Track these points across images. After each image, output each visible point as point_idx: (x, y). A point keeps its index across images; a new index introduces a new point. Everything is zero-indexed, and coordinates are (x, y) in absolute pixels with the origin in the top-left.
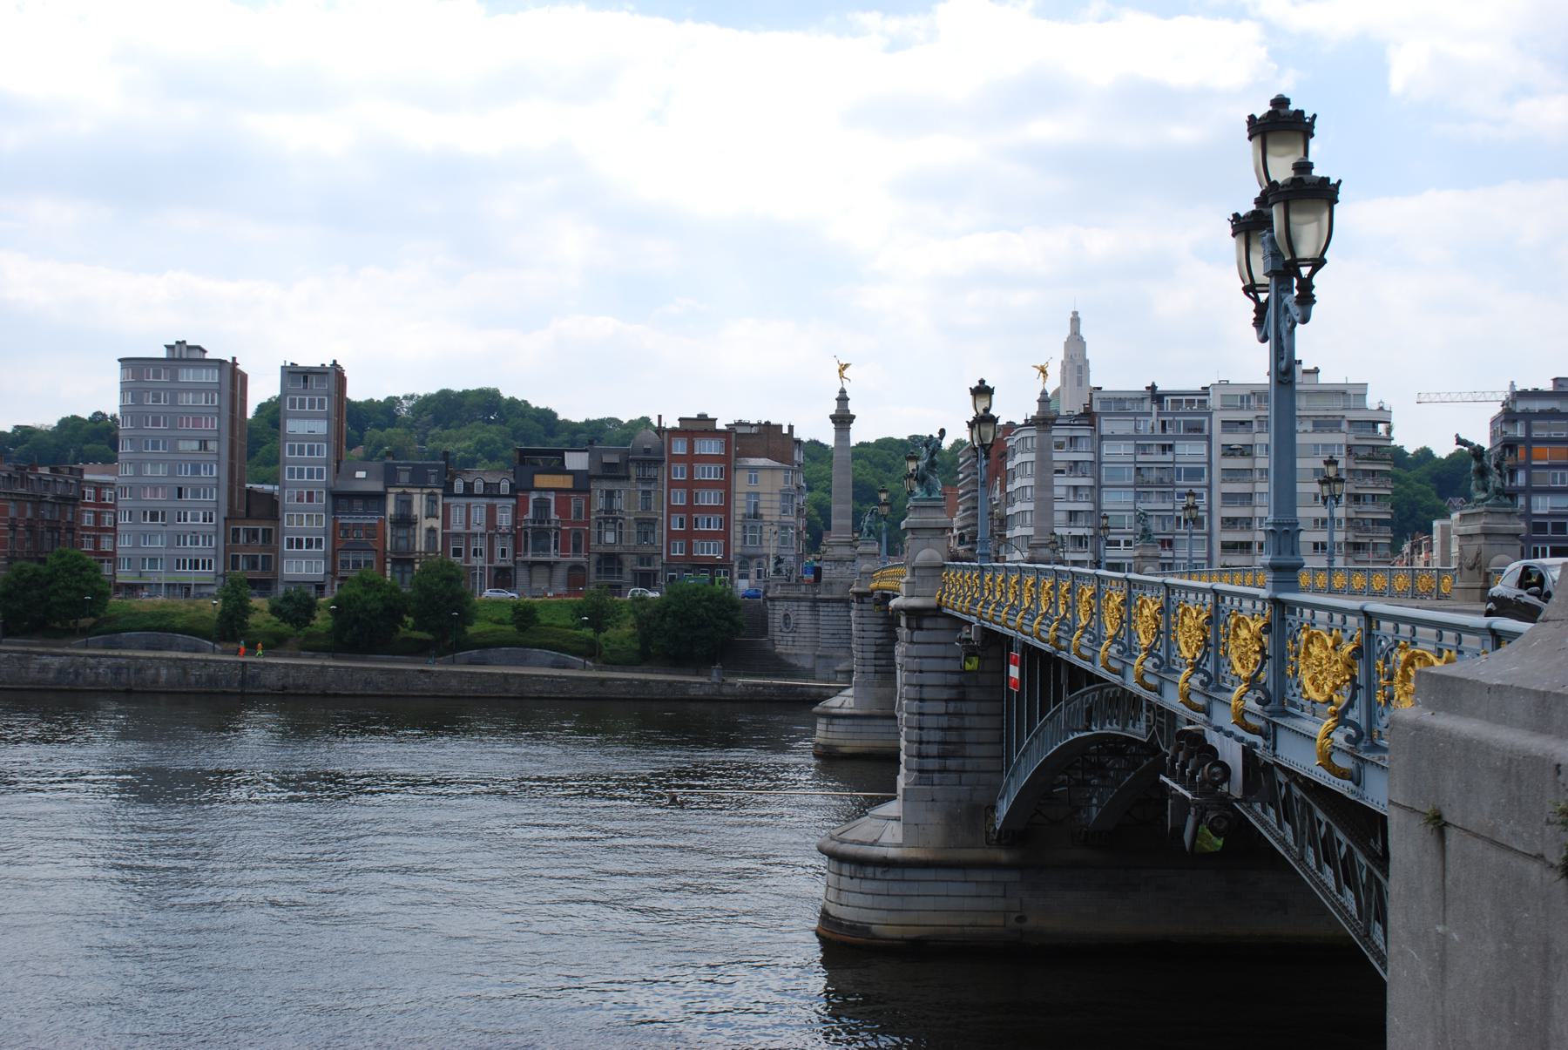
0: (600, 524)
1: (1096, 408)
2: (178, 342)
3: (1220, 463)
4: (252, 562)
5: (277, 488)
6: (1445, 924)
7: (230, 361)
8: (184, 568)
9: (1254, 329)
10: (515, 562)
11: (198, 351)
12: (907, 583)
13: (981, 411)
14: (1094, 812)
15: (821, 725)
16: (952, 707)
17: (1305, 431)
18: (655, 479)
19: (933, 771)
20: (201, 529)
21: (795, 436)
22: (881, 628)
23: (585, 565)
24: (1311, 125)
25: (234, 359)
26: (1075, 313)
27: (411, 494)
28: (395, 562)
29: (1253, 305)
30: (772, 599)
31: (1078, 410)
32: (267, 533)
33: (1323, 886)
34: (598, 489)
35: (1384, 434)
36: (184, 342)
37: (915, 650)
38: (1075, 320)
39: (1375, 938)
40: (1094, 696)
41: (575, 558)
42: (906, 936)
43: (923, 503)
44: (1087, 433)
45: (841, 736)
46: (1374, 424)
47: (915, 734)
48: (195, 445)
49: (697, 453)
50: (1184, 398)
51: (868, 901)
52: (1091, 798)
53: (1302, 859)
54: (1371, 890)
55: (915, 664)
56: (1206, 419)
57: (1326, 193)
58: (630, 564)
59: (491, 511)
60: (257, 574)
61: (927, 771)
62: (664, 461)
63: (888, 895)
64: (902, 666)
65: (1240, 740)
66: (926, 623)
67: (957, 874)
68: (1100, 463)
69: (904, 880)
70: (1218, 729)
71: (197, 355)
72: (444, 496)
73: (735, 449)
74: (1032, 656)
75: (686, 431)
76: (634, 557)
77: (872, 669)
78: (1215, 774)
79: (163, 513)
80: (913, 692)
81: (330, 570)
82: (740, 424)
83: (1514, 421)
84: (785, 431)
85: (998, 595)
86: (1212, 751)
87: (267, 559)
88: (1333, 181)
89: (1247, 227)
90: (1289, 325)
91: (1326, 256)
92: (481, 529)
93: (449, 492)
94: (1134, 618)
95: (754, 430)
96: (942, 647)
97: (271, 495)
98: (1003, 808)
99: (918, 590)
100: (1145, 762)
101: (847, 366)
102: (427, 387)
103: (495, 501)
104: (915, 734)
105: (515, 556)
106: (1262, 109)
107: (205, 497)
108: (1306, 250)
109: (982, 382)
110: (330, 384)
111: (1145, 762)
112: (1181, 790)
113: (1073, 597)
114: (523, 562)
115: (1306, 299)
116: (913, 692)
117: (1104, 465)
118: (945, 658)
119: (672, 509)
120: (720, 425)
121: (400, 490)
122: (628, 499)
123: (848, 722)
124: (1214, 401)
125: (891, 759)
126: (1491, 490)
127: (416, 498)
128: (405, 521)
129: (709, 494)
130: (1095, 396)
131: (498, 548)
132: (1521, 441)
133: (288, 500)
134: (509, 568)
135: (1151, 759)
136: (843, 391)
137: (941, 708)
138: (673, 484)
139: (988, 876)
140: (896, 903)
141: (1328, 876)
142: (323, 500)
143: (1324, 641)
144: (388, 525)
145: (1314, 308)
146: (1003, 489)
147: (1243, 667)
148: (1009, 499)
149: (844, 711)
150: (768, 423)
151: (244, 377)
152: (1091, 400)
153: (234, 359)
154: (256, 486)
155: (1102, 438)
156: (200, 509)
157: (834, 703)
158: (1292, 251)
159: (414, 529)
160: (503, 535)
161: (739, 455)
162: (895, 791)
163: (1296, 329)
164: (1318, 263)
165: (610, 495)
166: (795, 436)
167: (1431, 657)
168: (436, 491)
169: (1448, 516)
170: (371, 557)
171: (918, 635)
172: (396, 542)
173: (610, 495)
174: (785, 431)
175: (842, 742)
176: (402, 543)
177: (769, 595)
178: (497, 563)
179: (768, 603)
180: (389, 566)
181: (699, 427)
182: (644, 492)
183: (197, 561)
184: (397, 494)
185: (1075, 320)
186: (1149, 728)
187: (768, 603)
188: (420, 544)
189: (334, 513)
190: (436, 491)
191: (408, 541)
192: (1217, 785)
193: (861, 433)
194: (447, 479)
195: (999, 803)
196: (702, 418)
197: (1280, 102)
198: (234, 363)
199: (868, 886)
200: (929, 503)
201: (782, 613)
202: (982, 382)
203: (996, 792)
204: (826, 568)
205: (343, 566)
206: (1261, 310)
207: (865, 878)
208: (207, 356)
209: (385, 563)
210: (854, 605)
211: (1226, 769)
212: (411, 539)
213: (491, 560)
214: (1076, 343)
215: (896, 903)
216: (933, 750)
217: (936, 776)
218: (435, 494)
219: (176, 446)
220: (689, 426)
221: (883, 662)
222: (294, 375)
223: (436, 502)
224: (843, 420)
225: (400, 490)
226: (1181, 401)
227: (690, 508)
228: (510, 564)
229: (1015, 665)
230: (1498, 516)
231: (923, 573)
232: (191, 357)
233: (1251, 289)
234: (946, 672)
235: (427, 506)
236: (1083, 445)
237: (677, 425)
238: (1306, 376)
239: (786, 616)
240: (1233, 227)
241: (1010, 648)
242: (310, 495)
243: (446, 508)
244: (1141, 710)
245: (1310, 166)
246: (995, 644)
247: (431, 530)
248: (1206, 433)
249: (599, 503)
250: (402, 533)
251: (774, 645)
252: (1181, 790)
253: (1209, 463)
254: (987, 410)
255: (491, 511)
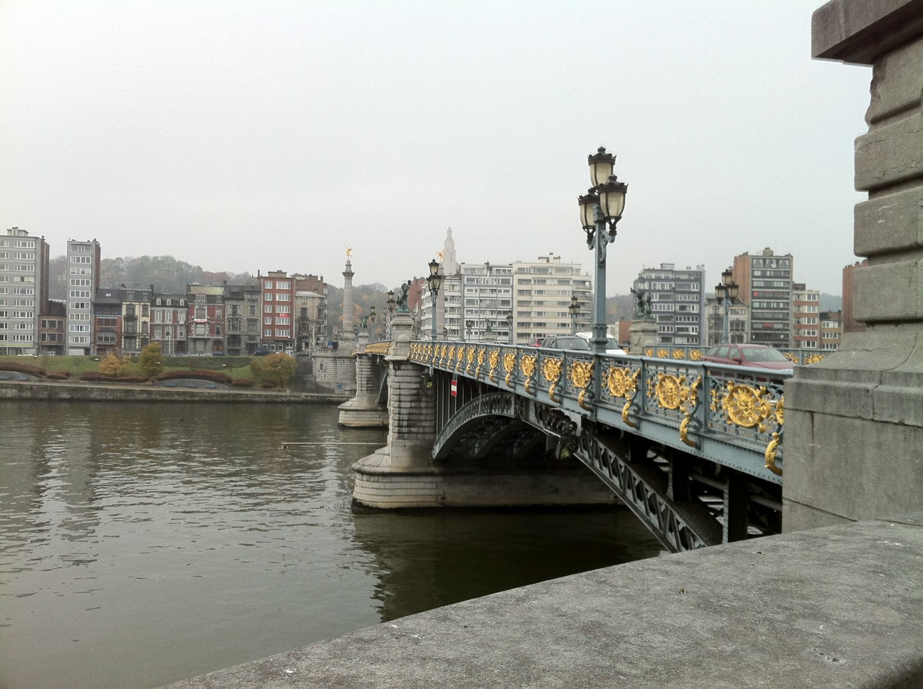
0: (230, 321)
1: (462, 272)
2: (13, 228)
3: (517, 298)
4: (53, 337)
5: (65, 301)
6: (813, 442)
7: (41, 238)
8: (18, 339)
9: (587, 244)
10: (188, 339)
11: (23, 232)
12: (394, 349)
13: (434, 274)
14: (477, 451)
15: (342, 414)
16: (413, 405)
17: (554, 285)
18: (257, 300)
19: (405, 433)
20: (26, 320)
21: (324, 282)
22: (369, 370)
23: (222, 341)
24: (614, 160)
25: (43, 237)
26: (450, 228)
27: (134, 305)
28: (126, 338)
29: (587, 234)
30: (314, 357)
31: (454, 273)
32: (60, 323)
33: (604, 476)
34: (229, 306)
35: (588, 286)
36: (17, 228)
37: (397, 379)
38: (450, 232)
39: (627, 496)
40: (486, 399)
41: (217, 337)
42: (392, 507)
43: (401, 314)
44: (459, 284)
45: (352, 419)
46: (584, 282)
47: (397, 417)
48: (19, 279)
49: (277, 288)
50: (501, 269)
51: (376, 492)
52: (474, 444)
53: (592, 465)
54: (626, 476)
55: (397, 385)
56: (511, 278)
57: (621, 189)
58: (244, 340)
59: (175, 314)
60: (54, 343)
61: (403, 433)
62: (261, 292)
63: (385, 489)
64: (391, 387)
65: (579, 413)
66: (402, 367)
67: (415, 479)
68: (464, 297)
69: (391, 482)
70: (568, 409)
71: (23, 234)
72: (151, 306)
73: (295, 287)
74: (462, 381)
75: (272, 278)
76: (247, 337)
77: (366, 389)
78: (570, 427)
79: (6, 313)
80: (396, 398)
81: (92, 341)
82: (296, 275)
83: (644, 282)
84: (319, 279)
85: (419, 351)
86: (568, 418)
87: (60, 336)
88: (625, 185)
89: (587, 201)
90: (604, 243)
91: (622, 215)
92: (170, 323)
93: (153, 304)
94: (520, 364)
95: (304, 278)
96: (409, 378)
97: (61, 304)
98: (437, 449)
99: (399, 352)
100: (502, 428)
101: (350, 250)
102: (136, 254)
103: (177, 309)
104: (397, 417)
105: (187, 335)
106: (595, 152)
107: (28, 305)
108: (613, 212)
109: (434, 260)
110: (92, 251)
111: (502, 428)
112: (554, 434)
113: (486, 356)
114: (191, 338)
115: (613, 232)
116: (396, 398)
117: (466, 320)
118: (411, 383)
119: (265, 315)
120: (288, 276)
121: (128, 303)
122: (243, 310)
123: (354, 413)
124: (515, 269)
125: (385, 428)
126: (645, 312)
127: (137, 308)
128: (131, 318)
129: (283, 308)
130: (462, 266)
131: (178, 332)
132: (647, 290)
133: (71, 309)
134: (185, 341)
135: (505, 427)
136: (349, 262)
137: (408, 405)
138: (265, 303)
139: (429, 479)
140: (388, 492)
141: (606, 471)
142: (88, 309)
143: (620, 372)
144: (123, 320)
145: (616, 237)
146: (420, 308)
147: (579, 383)
148: (422, 312)
149: (353, 408)
150: (310, 276)
151: (48, 246)
152: (460, 269)
153: (43, 237)
154: (53, 300)
155: (465, 286)
156: (26, 311)
157: (347, 405)
158: (608, 213)
159: (136, 322)
160: (181, 325)
161: (297, 290)
162: (386, 442)
163: (607, 245)
164: (618, 218)
165: (235, 307)
166: (324, 282)
167: (674, 378)
168: (147, 304)
169: (614, 323)
170: (114, 335)
171: (398, 373)
172: (127, 329)
173: (235, 307)
174: (319, 279)
175: (351, 422)
176: (130, 330)
177: (313, 355)
178: (178, 339)
179: (313, 359)
180: (123, 340)
181: (278, 276)
182: (251, 306)
183: (24, 337)
184: (127, 305)
185: (450, 232)
186: (516, 412)
187: (313, 359)
188: (139, 329)
189: (95, 313)
190: (147, 304)
191: (133, 328)
192: (571, 431)
193: (356, 282)
194: (153, 298)
195: (435, 447)
196: (279, 272)
197: (602, 150)
198: (43, 239)
199: (376, 485)
200: (404, 314)
201: (319, 363)
202: (434, 260)
203: (431, 444)
204: (340, 343)
205: (99, 340)
206: (590, 237)
207: (374, 481)
208: (29, 235)
209: (121, 338)
210: (358, 359)
211: (575, 424)
212: (135, 326)
213: (175, 337)
214: (450, 240)
215: (388, 492)
216: (405, 423)
217: (406, 436)
218: (147, 305)
219: (13, 279)
220: (273, 275)
221: (371, 385)
222: (74, 245)
223: (147, 309)
224: (349, 275)
225: (128, 303)
226: (500, 270)
227: (273, 315)
228: (184, 339)
229: (454, 385)
230: (648, 323)
231: (401, 345)
232: (21, 235)
233: (586, 227)
234: (411, 389)
235: (143, 312)
236: (457, 288)
237: (267, 275)
238: (555, 260)
239: (321, 365)
240: (579, 201)
241: (451, 378)
242: (82, 305)
243: (152, 312)
244: (511, 404)
245: (615, 178)
246: (442, 377)
247: (145, 323)
248: (511, 284)
249: (229, 311)
250: (130, 324)
251: (316, 378)
252: (554, 434)
253: (512, 298)
254: (436, 273)
255: (175, 314)
